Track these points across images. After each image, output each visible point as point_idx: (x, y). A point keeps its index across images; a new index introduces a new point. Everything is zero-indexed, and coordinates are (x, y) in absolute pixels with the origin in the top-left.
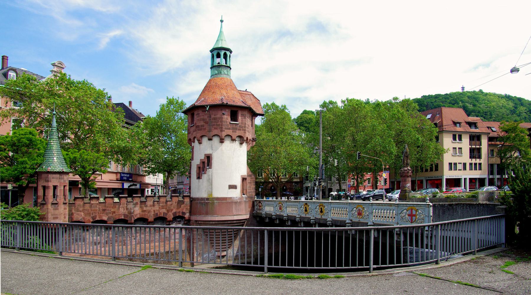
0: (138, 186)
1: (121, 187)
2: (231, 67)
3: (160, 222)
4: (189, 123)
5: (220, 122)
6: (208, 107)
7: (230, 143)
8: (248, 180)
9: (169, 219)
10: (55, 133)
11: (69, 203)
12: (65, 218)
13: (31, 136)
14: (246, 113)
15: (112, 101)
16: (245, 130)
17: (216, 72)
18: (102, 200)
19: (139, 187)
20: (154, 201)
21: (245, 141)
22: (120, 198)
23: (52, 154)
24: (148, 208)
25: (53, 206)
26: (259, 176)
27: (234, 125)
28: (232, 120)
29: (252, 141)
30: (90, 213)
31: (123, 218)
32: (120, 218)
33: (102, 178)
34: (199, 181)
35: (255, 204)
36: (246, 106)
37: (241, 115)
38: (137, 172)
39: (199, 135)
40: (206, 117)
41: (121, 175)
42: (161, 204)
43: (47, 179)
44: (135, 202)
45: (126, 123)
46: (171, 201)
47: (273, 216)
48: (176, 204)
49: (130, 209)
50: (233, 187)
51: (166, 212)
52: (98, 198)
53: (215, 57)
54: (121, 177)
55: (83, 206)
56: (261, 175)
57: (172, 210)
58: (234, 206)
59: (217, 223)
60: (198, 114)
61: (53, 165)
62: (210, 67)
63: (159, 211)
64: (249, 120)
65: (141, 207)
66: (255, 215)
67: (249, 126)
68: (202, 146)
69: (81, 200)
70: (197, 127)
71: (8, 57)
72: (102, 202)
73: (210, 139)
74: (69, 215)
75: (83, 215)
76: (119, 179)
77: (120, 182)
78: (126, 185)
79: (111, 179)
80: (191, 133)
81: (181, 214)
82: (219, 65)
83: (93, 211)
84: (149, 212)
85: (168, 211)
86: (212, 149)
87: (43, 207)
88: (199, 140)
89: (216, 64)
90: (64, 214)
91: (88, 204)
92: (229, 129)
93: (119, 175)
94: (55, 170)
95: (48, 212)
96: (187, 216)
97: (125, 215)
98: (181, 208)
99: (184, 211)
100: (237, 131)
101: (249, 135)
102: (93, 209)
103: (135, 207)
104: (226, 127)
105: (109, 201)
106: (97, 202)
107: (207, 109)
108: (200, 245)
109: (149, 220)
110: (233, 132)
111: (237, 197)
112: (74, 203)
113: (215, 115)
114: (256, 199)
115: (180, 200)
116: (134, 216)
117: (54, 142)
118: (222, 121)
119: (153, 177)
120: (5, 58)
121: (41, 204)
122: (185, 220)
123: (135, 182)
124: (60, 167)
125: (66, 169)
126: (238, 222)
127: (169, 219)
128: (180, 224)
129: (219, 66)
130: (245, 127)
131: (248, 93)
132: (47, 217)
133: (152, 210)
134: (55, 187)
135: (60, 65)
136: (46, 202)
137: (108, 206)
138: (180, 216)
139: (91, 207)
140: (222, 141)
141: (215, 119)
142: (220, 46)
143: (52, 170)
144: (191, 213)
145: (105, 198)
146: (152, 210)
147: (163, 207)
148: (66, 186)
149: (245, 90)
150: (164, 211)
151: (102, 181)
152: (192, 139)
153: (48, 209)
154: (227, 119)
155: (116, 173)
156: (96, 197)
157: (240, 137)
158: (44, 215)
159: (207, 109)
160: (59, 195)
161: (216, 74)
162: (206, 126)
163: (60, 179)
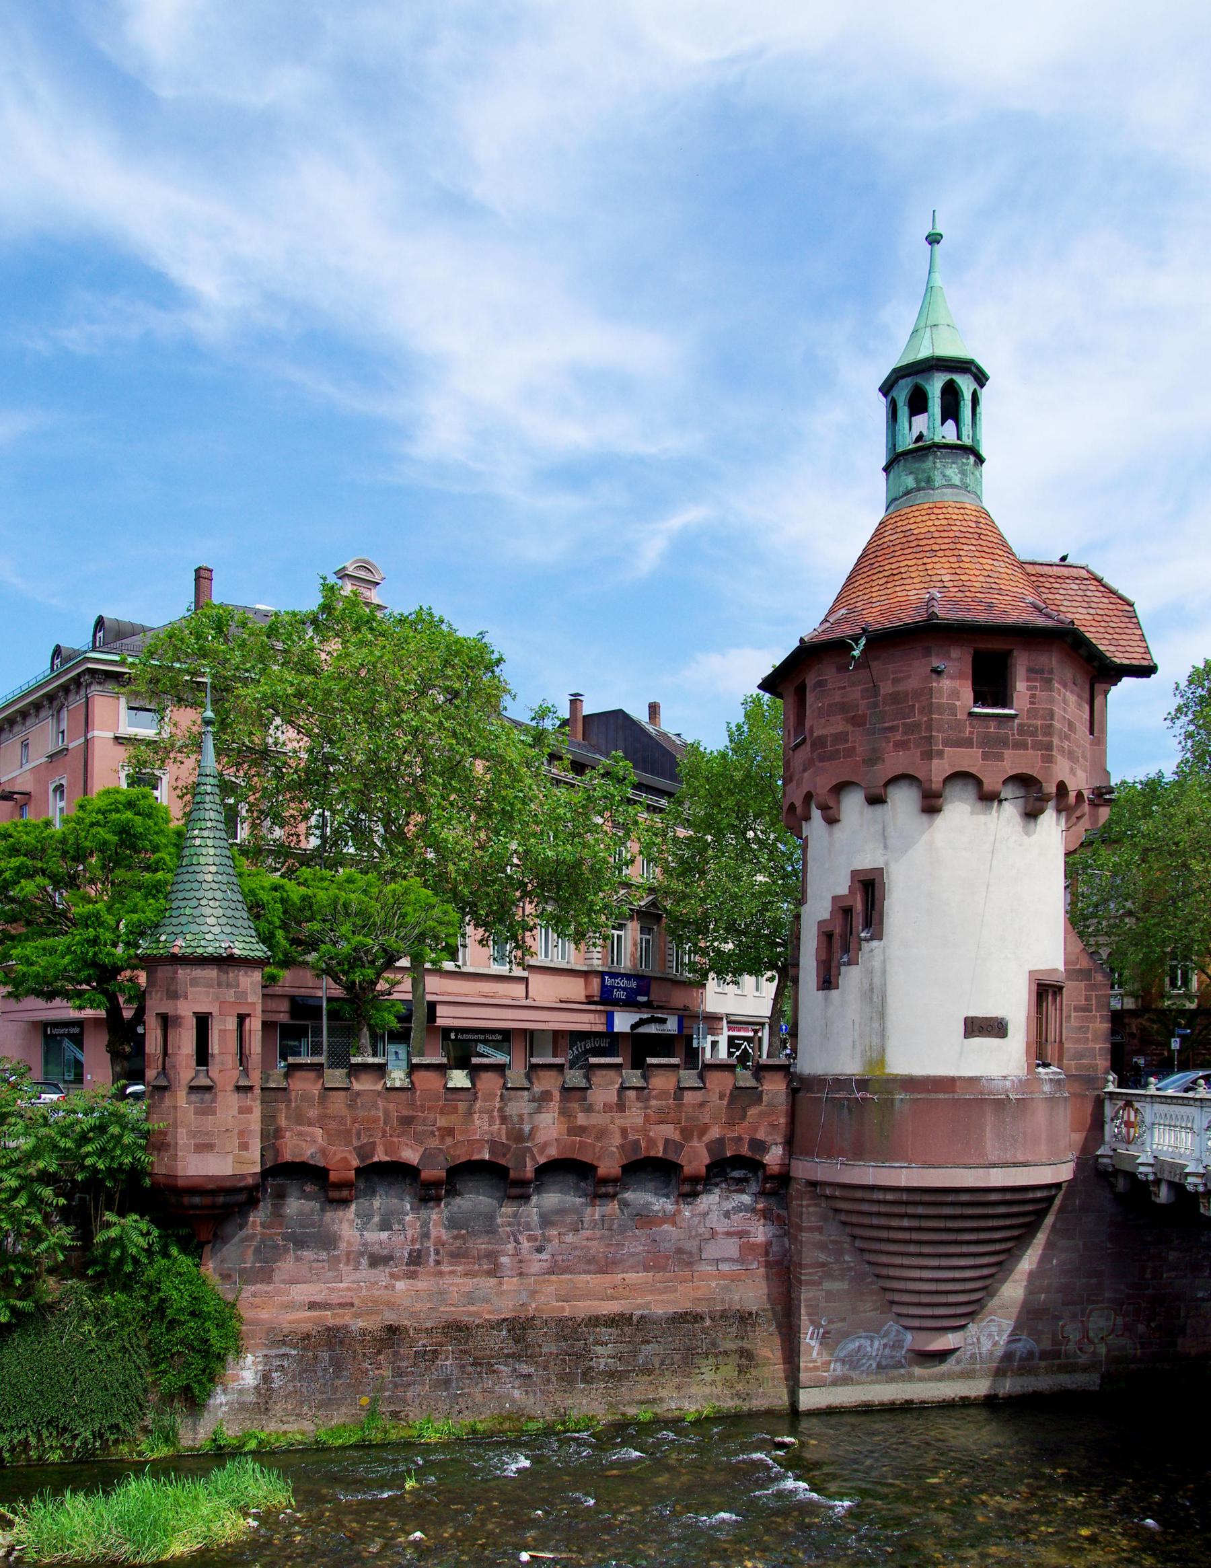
0: (671, 1026)
1: (601, 1028)
2: (984, 452)
3: (651, 1181)
4: (789, 731)
5: (922, 711)
6: (863, 641)
7: (972, 813)
8: (1073, 993)
9: (688, 1170)
10: (208, 798)
11: (262, 1089)
12: (244, 1147)
13: (129, 815)
14: (1053, 660)
15: (722, 748)
16: (1049, 747)
17: (910, 482)
18: (397, 1077)
19: (676, 1027)
20: (623, 1088)
21: (1052, 804)
22: (474, 1071)
23: (195, 885)
24: (596, 1119)
25: (195, 1097)
26: (1173, 985)
27: (993, 724)
28: (980, 697)
29: (1094, 805)
30: (349, 1132)
31: (487, 1157)
32: (476, 1157)
33: (530, 995)
34: (826, 999)
35: (1109, 1110)
36: (1050, 623)
37: (1030, 670)
38: (669, 971)
39: (822, 785)
40: (855, 694)
41: (603, 981)
42: (653, 1102)
43: (172, 988)
44: (537, 1089)
45: (638, 787)
46: (701, 1088)
47: (1190, 1180)
48: (725, 1102)
49: (515, 1119)
50: (992, 1028)
51: (677, 1136)
52: (381, 1070)
53: (903, 411)
54: (606, 992)
55: (323, 1100)
56: (1186, 982)
57: (703, 1130)
58: (990, 1119)
59: (905, 1197)
60: (821, 684)
61: (194, 928)
62: (883, 463)
63: (645, 1131)
64: (1072, 698)
65: (564, 1112)
66: (1106, 1165)
67: (1071, 726)
68: (842, 832)
69: (312, 1075)
70: (819, 743)
71: (211, 571)
72: (398, 1084)
73: (875, 800)
74: (264, 1136)
75: (320, 1140)
76: (596, 999)
77: (599, 1008)
78: (623, 1022)
79: (564, 998)
80: (796, 777)
81: (745, 1151)
82: (920, 444)
83: (361, 1123)
84: (602, 1134)
85: (687, 1134)
86: (885, 847)
87: (162, 1099)
88: (824, 808)
89: (906, 442)
90: (241, 1134)
91: (343, 1093)
92: (968, 743)
93: (596, 982)
94: (200, 951)
95: (175, 1119)
96: (774, 1157)
97: (493, 1144)
98: (745, 1124)
99: (761, 1135)
100: (1008, 753)
101: (1072, 771)
102: (361, 1113)
103: (539, 1111)
104: (953, 735)
105: (429, 1081)
106: (379, 1087)
107: (856, 653)
108: (830, 1297)
109: (602, 1171)
110: (985, 756)
111: (1005, 1078)
112: (284, 1089)
113: (896, 681)
114: (1111, 1088)
115: (741, 1084)
116: (535, 1150)
117: (205, 834)
118: (929, 709)
119: (720, 990)
120: (204, 574)
121: (154, 1086)
122: (768, 1178)
123: (660, 1007)
124: (223, 937)
125: (247, 946)
126: (1008, 1197)
127: (688, 1170)
128: (742, 1191)
129: (925, 450)
130: (1048, 730)
131: (1074, 572)
132: (173, 1143)
133: (614, 1128)
134: (203, 1022)
135: (362, 574)
136: (169, 1081)
137: (422, 1106)
138: (743, 1157)
139: (352, 1105)
140: (934, 802)
141: (895, 698)
142: (924, 353)
143: (189, 950)
144: (790, 1144)
145: (413, 1069)
146: (614, 1128)
147: (662, 1117)
148: (249, 1015)
149: (1056, 560)
150: (669, 1131)
151: (529, 1002)
152: (798, 803)
153: (175, 1107)
154: (955, 694)
155: (586, 974)
156: (373, 1065)
157: (1025, 781)
158: (163, 1133)
159: (856, 653)
160: (216, 1051)
161: (908, 493)
162: (859, 742)
163: (219, 985)
